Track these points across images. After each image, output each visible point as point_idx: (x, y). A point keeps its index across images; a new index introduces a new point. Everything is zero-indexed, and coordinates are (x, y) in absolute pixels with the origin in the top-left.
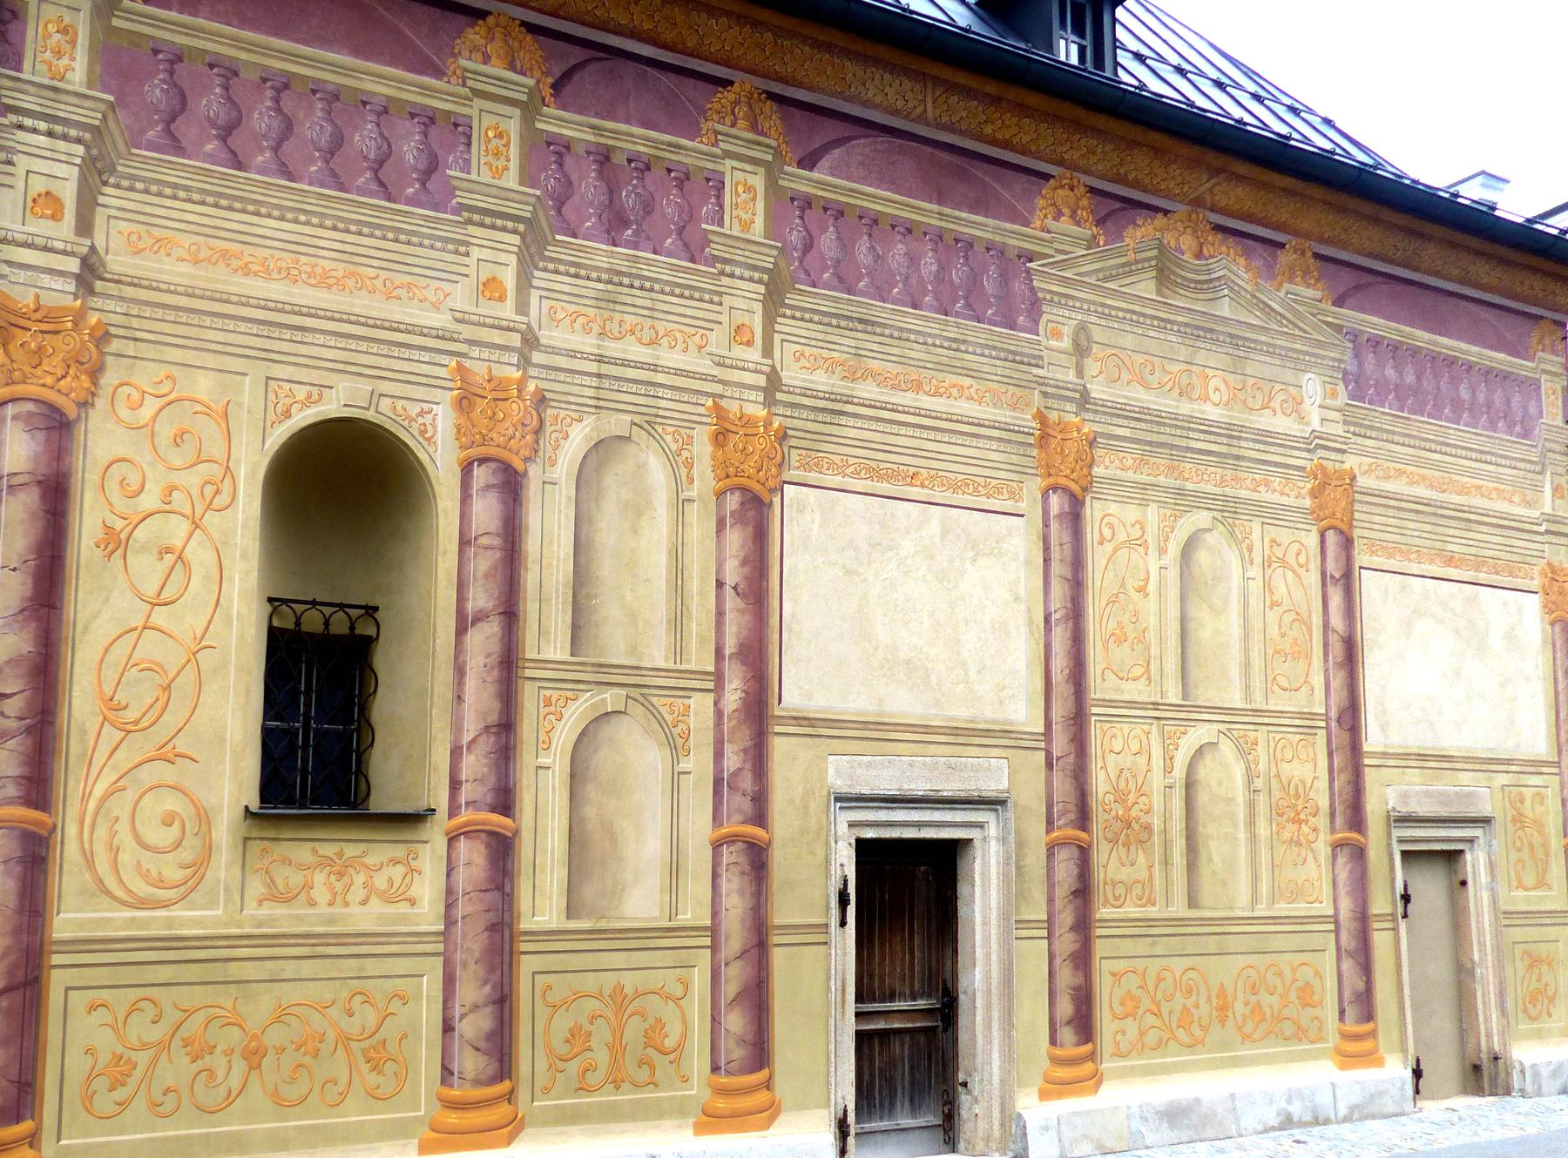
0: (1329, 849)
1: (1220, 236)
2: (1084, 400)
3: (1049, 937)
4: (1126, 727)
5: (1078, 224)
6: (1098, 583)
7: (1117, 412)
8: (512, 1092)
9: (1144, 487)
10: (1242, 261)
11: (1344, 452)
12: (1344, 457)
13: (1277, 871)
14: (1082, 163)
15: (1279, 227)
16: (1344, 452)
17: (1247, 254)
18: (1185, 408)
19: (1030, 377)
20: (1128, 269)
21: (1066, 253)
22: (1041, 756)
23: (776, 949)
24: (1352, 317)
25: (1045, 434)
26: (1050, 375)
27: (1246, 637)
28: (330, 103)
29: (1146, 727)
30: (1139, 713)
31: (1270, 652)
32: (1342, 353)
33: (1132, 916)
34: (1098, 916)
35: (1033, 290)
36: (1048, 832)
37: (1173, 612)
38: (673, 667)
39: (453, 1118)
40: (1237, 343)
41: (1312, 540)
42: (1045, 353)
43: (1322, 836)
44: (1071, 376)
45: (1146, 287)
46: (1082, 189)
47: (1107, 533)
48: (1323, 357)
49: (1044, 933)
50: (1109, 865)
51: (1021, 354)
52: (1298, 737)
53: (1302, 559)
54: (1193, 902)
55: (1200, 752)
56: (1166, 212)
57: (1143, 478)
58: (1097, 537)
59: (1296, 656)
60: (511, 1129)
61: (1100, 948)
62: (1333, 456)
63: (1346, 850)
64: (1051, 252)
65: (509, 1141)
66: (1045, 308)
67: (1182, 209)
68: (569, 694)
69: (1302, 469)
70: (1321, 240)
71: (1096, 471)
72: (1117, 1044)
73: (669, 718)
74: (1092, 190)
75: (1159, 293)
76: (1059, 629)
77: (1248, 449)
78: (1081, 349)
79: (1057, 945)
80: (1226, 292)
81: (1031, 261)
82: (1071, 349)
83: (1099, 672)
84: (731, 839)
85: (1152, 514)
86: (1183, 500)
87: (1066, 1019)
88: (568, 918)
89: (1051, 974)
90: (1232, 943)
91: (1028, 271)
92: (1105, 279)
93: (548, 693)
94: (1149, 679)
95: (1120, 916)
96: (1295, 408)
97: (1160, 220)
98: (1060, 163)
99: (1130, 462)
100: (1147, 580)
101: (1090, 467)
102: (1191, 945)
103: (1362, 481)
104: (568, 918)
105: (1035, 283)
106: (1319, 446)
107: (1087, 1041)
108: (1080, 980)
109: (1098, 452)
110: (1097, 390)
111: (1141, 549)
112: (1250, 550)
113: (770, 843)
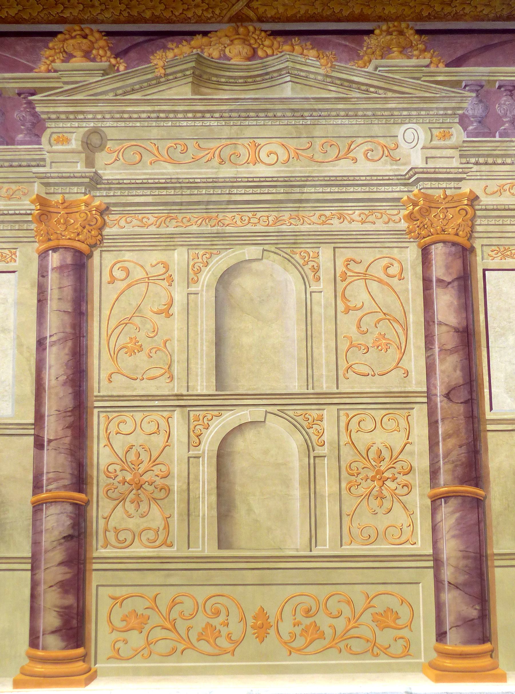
0: (429, 502)
1: (279, 39)
2: (95, 182)
3: (33, 570)
4: (139, 416)
5: (94, 60)
6: (106, 312)
7: (122, 185)
8: (492, 651)
9: (171, 236)
10: (313, 53)
11: (460, 180)
12: (460, 184)
13: (346, 520)
14: (100, 17)
15: (362, 18)
16: (460, 180)
17: (318, 46)
18: (227, 172)
19: (31, 175)
20: (165, 79)
21: (77, 82)
22: (31, 440)
23: (94, 573)
24: (474, 72)
25: (45, 211)
26: (54, 170)
27: (309, 337)
28: (477, 91)
29: (165, 414)
30: (157, 403)
31: (343, 346)
32: (469, 103)
33: (143, 555)
34: (95, 555)
35: (35, 115)
36: (34, 494)
37: (205, 323)
38: (306, 391)
39: (39, 668)
40: (298, 113)
41: (411, 254)
42: (47, 156)
43: (416, 491)
44: (80, 167)
45: (183, 90)
46: (97, 35)
47: (118, 274)
48: (431, 109)
49: (29, 566)
50: (107, 515)
51: (24, 160)
52: (384, 412)
53: (394, 270)
54: (223, 541)
55: (240, 428)
56: (205, 34)
57: (170, 230)
58: (106, 277)
59: (382, 344)
60: (90, 676)
61: (95, 579)
62: (452, 184)
63: (453, 503)
64: (61, 85)
65: (87, 684)
66: (48, 125)
67: (227, 28)
68: (216, 413)
69: (398, 200)
70: (420, 18)
71: (107, 231)
72: (137, 653)
73: (305, 424)
74: (109, 34)
75: (194, 93)
76: (54, 349)
77: (311, 193)
78: (93, 144)
79: (42, 575)
80: (288, 79)
81: (33, 94)
82: (80, 148)
83: (104, 375)
84: (447, 497)
85: (178, 257)
86: (221, 240)
87: (50, 629)
88: (219, 548)
89: (33, 597)
90: (279, 576)
91: (30, 103)
92: (125, 93)
93: (198, 413)
94: (171, 378)
95: (127, 555)
96: (390, 153)
97: (198, 40)
98: (63, 21)
99: (152, 219)
100: (171, 304)
101: (101, 229)
102: (219, 577)
103: (485, 200)
104: (219, 548)
105: (38, 109)
106: (418, 180)
107: (78, 646)
108: (70, 600)
109: (109, 218)
110: (107, 174)
111: (165, 283)
112: (316, 270)
113: (485, 498)
